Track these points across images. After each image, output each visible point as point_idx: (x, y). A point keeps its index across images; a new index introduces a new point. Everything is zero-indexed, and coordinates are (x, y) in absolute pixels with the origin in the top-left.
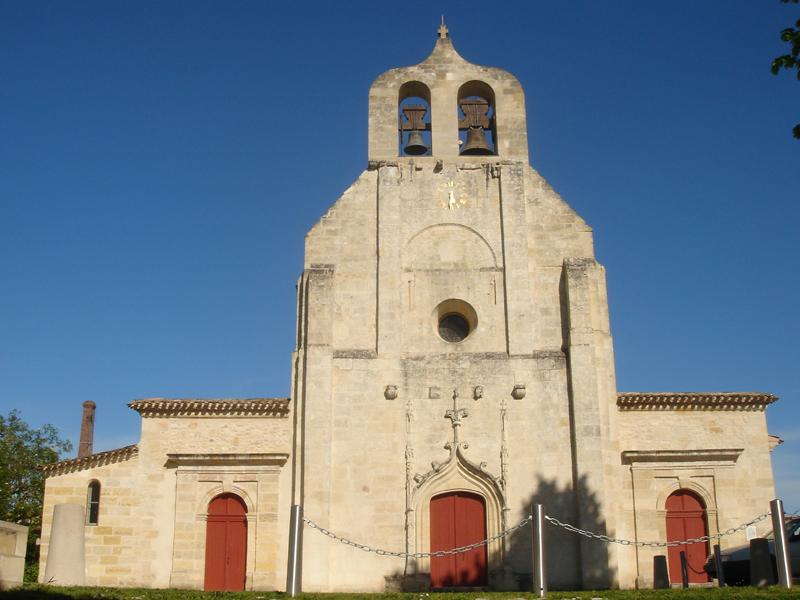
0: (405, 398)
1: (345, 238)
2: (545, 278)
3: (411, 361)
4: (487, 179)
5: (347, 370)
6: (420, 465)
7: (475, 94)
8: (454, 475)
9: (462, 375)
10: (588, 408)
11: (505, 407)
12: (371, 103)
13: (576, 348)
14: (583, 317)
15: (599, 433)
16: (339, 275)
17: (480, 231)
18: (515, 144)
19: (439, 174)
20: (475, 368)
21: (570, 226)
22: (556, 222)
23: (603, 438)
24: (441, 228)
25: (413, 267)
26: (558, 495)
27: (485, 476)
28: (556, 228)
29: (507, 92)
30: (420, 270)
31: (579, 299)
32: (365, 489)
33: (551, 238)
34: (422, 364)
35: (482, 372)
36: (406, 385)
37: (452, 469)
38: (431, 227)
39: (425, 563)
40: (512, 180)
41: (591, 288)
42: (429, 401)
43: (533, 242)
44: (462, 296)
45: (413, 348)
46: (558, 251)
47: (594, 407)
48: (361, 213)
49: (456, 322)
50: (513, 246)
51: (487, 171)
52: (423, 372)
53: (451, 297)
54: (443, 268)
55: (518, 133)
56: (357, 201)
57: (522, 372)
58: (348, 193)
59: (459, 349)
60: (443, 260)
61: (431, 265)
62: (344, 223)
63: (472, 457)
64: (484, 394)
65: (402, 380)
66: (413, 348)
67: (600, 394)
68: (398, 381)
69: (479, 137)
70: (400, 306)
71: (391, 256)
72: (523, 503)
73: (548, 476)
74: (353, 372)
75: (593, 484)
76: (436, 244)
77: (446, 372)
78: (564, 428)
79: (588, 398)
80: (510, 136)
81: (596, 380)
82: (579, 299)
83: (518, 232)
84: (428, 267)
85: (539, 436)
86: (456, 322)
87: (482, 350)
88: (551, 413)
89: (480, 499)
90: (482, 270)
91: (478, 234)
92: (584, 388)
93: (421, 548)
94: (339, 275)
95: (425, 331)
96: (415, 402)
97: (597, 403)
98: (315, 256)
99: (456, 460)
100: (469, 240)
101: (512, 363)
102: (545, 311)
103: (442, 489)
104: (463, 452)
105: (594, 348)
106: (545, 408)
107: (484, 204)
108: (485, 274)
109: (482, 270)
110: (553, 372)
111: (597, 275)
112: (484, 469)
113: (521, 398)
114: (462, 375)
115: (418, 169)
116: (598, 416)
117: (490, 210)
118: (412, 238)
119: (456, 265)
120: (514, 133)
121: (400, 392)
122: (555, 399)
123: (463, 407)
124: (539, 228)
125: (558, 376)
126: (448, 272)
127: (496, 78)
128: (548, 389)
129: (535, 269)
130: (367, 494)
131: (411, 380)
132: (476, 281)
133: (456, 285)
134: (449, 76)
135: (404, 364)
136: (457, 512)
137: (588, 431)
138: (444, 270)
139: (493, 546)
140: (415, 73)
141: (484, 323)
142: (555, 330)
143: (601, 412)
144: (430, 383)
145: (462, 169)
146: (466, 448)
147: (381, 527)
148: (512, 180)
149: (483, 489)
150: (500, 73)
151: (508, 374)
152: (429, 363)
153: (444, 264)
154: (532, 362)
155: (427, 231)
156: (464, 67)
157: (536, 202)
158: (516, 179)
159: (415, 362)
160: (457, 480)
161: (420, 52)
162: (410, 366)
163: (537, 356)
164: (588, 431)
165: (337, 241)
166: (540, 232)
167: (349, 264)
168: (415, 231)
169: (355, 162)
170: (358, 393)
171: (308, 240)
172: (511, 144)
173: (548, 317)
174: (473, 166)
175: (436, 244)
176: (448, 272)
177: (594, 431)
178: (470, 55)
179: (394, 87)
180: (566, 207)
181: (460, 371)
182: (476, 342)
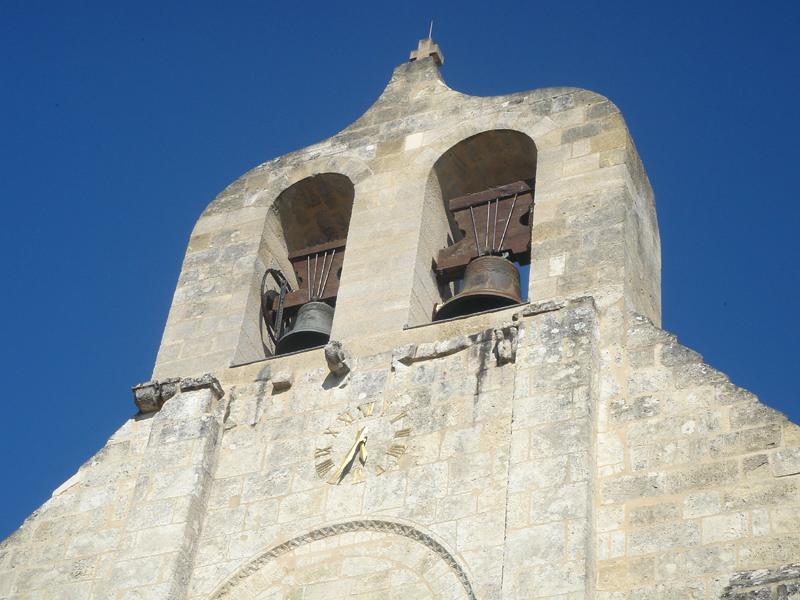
4: (482, 372)
7: (489, 180)
12: (192, 253)
17: (436, 533)
18: (581, 262)
19: (336, 390)
21: (763, 461)
22: (707, 460)
24: (320, 545)
28: (703, 479)
29: (571, 136)
33: (687, 514)
38: (285, 546)
40: (549, 353)
43: (620, 537)
46: (712, 551)
48: (83, 540)
50: (535, 551)
51: (484, 351)
55: (597, 230)
56: (83, 508)
58: (62, 495)
69: (480, 270)
80: (570, 245)
83: (554, 507)
90: (342, 477)
91: (431, 543)
100: (400, 566)
107: (460, 449)
111: (340, 134)
115: (282, 387)
117: (479, 458)
120: (583, 233)
124: (643, 486)
127: (545, 110)
134: (413, 142)
140: (322, 157)
145: (407, 361)
148: (549, 353)
150: (554, 96)
155: (272, 563)
156: (456, 110)
157: (641, 409)
158: (565, 347)
161: (345, 101)
166: (647, 501)
169: (108, 383)
172: (571, 263)
174: (443, 346)
178: (468, 74)
179: (260, 201)
180: (749, 403)
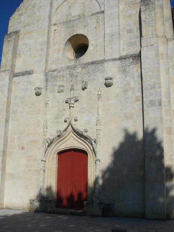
0: (46, 94)
1: (26, 16)
2: (130, 12)
3: (50, 72)
5: (19, 83)
6: (52, 133)
8: (70, 138)
9: (76, 76)
10: (153, 87)
11: (100, 93)
13: (145, 49)
14: (150, 28)
15: (160, 104)
16: (21, 34)
20: (84, 71)
23: (164, 108)
25: (58, 22)
26: (139, 142)
27: (86, 138)
30: (60, 23)
31: (147, 17)
32: (23, 148)
34: (55, 73)
35: (88, 73)
36: (46, 86)
37: (68, 135)
39: (54, 189)
41: (158, 10)
42: (58, 94)
44: (81, 32)
45: (54, 65)
47: (157, 86)
49: (80, 46)
52: (55, 78)
53: (75, 34)
54: (72, 19)
57: (112, 70)
59: (78, 62)
60: (73, 15)
61: (67, 19)
62: (26, 9)
63: (80, 127)
64: (88, 87)
65: (45, 84)
66: (54, 65)
67: (162, 78)
68: (42, 85)
70: (94, 54)
71: (44, 18)
72: (114, 149)
73: (131, 131)
74: (21, 83)
75: (162, 135)
76: (70, 8)
77: (68, 76)
78: (138, 103)
79: (152, 80)
81: (159, 67)
82: (147, 17)
84: (65, 20)
85: (121, 110)
86: (80, 46)
87: (90, 61)
88: (130, 93)
89: (85, 153)
90: (93, 15)
92: (150, 74)
93: (50, 180)
94: (21, 34)
95: (60, 55)
96: (51, 96)
97: (159, 83)
98: (12, 28)
99: (70, 128)
101: (106, 64)
102: (130, 31)
103: (63, 146)
104: (73, 123)
105: (158, 47)
106: (125, 91)
108: (94, 17)
109: (93, 15)
110: (131, 67)
112: (85, 134)
113: (111, 86)
114: (76, 76)
116: (160, 92)
118: (58, 8)
119: (79, 16)
121: (43, 92)
122: (132, 84)
123: (75, 96)
125: (134, 69)
126: (74, 21)
128: (128, 78)
129: (124, 8)
130: (23, 151)
131: (49, 83)
132: (89, 22)
133: (78, 26)
135: (46, 75)
136: (72, 160)
137: (152, 103)
138: (73, 20)
139: (91, 180)
141: (92, 45)
142: (135, 42)
143: (163, 90)
144: (59, 84)
146: (76, 120)
147: (29, 170)
149: (86, 147)
151: (103, 72)
152: (59, 72)
153: (74, 17)
154: (118, 62)
159: (52, 73)
160: (72, 142)
162: (49, 75)
163: (121, 59)
164: (152, 103)
165: (22, 18)
167: (26, 28)
168: (59, 4)
170: (23, 94)
171: (10, 21)
173: (131, 35)
175: (70, 8)
176: (74, 21)
177: (157, 103)
181: (76, 74)
182: (87, 58)
